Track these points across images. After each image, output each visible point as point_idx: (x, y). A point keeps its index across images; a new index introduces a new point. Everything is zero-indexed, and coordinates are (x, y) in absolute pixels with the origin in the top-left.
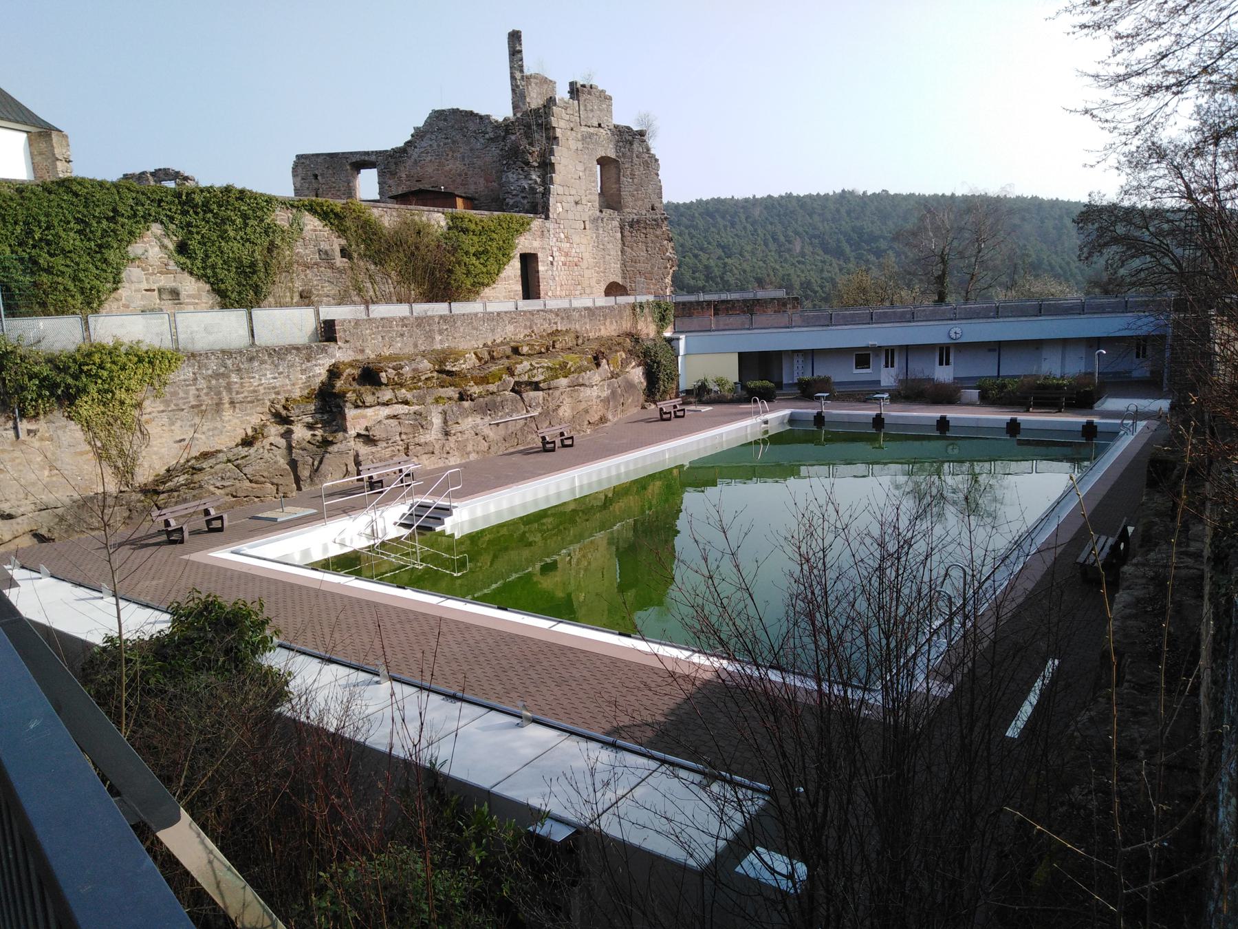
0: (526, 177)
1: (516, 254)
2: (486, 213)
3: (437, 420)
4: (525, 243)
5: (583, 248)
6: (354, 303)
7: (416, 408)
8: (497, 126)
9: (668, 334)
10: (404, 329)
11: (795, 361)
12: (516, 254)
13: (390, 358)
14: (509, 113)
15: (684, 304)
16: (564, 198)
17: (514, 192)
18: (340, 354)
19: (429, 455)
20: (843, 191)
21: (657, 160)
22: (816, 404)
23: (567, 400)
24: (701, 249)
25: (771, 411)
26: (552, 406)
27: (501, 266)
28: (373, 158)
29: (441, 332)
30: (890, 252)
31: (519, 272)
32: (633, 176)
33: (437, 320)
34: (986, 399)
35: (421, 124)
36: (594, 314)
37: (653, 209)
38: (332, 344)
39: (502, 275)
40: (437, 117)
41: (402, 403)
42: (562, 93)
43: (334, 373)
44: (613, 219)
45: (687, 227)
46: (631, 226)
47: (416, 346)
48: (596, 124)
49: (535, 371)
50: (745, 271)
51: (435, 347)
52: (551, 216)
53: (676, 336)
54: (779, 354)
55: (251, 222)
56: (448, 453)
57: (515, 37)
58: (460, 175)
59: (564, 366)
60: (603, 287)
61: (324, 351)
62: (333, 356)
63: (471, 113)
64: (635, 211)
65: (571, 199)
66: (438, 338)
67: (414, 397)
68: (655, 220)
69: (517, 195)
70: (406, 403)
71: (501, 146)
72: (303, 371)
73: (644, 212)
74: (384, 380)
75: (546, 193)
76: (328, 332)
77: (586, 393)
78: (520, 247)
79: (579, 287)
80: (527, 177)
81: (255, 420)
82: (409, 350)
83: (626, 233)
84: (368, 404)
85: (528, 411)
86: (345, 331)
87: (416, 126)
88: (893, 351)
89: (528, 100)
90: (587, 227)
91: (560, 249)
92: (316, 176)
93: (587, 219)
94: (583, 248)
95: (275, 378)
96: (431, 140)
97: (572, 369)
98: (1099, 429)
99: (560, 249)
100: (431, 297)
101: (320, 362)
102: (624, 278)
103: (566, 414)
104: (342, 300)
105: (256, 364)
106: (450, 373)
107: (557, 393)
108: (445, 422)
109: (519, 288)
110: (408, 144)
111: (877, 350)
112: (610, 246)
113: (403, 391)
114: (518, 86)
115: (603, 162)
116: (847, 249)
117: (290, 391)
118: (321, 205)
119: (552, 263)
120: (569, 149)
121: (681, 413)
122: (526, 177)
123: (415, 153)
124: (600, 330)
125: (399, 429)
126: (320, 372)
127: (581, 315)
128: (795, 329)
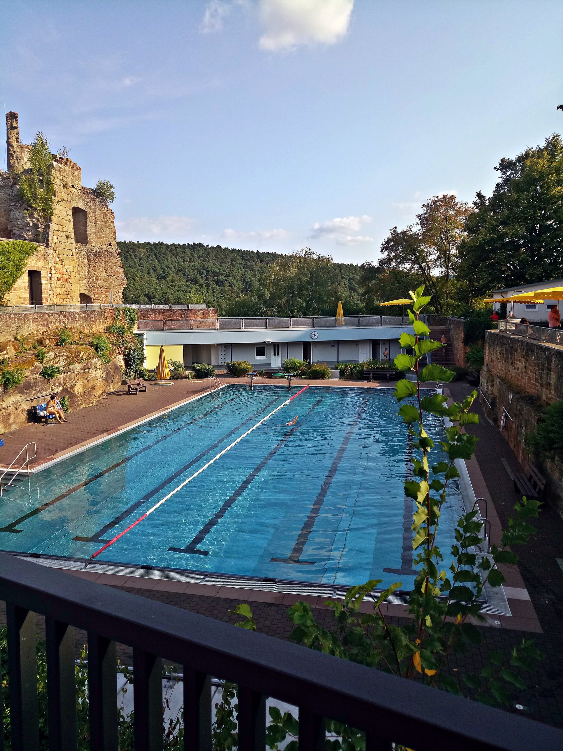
4: (32, 263)
9: (135, 330)
11: (220, 351)
12: (26, 270)
16: (59, 233)
17: (20, 226)
20: (194, 244)
23: (80, 381)
30: (226, 283)
31: (27, 284)
32: (96, 221)
34: (343, 375)
36: (88, 317)
39: (15, 286)
44: (82, 250)
46: (95, 255)
50: (137, 289)
52: (50, 245)
54: (208, 347)
65: (64, 234)
68: (111, 253)
78: (28, 265)
79: (69, 296)
83: (91, 260)
85: (52, 390)
91: (56, 269)
97: (84, 357)
99: (56, 269)
103: (79, 391)
107: (73, 375)
109: (27, 295)
111: (269, 344)
115: (76, 211)
116: (200, 279)
119: (50, 278)
124: (92, 327)
127: (80, 317)
128: (166, 331)
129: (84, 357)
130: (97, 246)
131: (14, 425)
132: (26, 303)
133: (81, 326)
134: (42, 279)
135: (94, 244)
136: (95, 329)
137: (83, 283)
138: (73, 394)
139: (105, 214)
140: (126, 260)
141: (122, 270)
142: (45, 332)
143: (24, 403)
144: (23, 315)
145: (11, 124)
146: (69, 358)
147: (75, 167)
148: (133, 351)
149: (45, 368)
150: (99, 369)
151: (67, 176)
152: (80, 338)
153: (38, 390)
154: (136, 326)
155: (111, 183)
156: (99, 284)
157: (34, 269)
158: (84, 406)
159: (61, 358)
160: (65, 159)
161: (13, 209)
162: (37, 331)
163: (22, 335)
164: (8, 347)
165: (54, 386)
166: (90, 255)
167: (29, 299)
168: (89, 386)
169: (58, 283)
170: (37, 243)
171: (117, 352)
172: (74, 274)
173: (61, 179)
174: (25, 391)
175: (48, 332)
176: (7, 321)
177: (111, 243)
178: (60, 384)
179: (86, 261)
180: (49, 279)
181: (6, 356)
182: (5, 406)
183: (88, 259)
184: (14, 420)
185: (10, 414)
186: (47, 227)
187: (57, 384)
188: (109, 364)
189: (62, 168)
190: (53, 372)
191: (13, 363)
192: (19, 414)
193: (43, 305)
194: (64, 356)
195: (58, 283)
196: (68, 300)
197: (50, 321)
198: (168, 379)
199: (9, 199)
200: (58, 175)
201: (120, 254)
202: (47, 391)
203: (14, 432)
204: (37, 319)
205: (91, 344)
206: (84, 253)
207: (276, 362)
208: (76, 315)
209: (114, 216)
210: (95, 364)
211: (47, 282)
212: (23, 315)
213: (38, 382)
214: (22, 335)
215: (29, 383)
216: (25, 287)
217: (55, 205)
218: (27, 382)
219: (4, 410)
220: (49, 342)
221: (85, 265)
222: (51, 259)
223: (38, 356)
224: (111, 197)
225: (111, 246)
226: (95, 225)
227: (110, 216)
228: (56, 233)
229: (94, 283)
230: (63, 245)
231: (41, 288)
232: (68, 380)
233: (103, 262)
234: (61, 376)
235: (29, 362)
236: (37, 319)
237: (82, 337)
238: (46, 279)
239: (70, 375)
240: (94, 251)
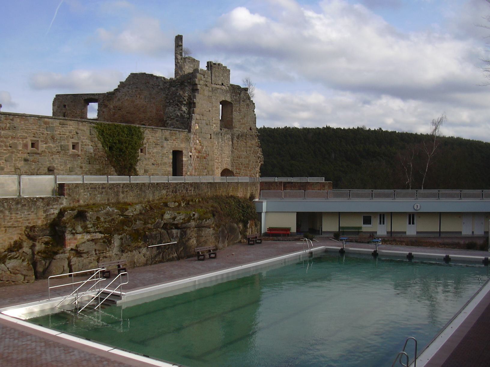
0: (179, 109)
6: (76, 174)
14: (173, 76)
15: (266, 183)
18: (65, 202)
21: (254, 104)
22: (373, 245)
25: (315, 246)
28: (97, 97)
29: (123, 192)
33: (122, 186)
35: (124, 80)
37: (250, 129)
40: (133, 77)
42: (203, 66)
43: (62, 213)
48: (221, 83)
57: (179, 39)
58: (142, 107)
62: (62, 204)
63: (152, 75)
69: (174, 119)
71: (166, 93)
75: (190, 118)
76: (61, 189)
79: (206, 171)
80: (180, 109)
81: (16, 238)
83: (235, 142)
88: (384, 215)
89: (184, 70)
90: (212, 137)
91: (195, 149)
92: (65, 106)
93: (212, 133)
95: (29, 214)
96: (129, 88)
98: (451, 259)
100: (120, 173)
101: (55, 207)
104: (71, 171)
105: (20, 206)
109: (171, 169)
110: (116, 90)
114: (178, 63)
120: (204, 95)
121: (213, 255)
122: (179, 109)
123: (119, 95)
126: (54, 211)
130: (240, 130)
134: (184, 157)
135: (238, 129)
139: (248, 105)
141: (260, 150)
145: (178, 44)
156: (240, 161)
167: (172, 172)
169: (197, 160)
177: (252, 127)
179: (231, 143)
183: (232, 141)
195: (197, 160)
207: (381, 230)
216: (169, 163)
225: (251, 130)
229: (237, 160)
238: (187, 157)
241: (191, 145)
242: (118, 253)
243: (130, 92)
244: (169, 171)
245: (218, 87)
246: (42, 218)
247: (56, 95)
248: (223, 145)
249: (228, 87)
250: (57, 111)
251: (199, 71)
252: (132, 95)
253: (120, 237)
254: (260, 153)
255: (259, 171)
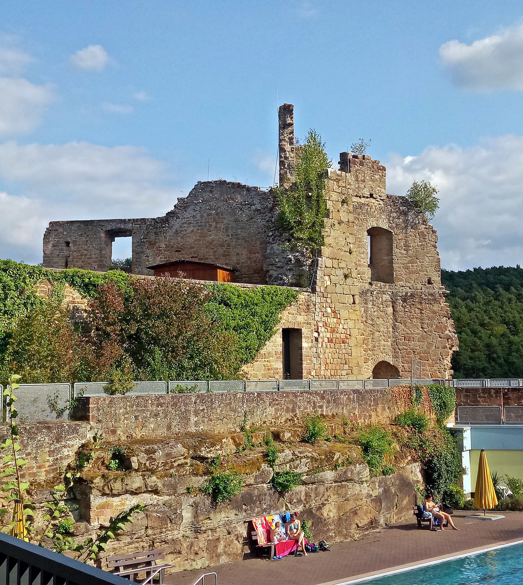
1: (279, 328)
2: (249, 285)
3: (187, 515)
5: (351, 324)
7: (166, 498)
8: (263, 196)
9: (450, 424)
10: (159, 408)
12: (279, 328)
13: (143, 441)
15: (467, 390)
17: (279, 264)
19: (175, 556)
24: (482, 325)
26: (313, 504)
27: (262, 340)
28: (129, 226)
29: (196, 413)
31: (280, 349)
32: (407, 247)
36: (363, 399)
38: (84, 424)
39: (262, 352)
41: (151, 492)
44: (384, 293)
45: (464, 299)
46: (404, 300)
47: (169, 428)
48: (367, 194)
49: (298, 462)
51: (189, 430)
52: (318, 289)
53: (459, 426)
55: (13, 293)
56: (197, 554)
58: (222, 245)
59: (329, 456)
60: (371, 366)
61: (75, 431)
62: (84, 437)
64: (408, 284)
65: (340, 273)
66: (193, 419)
67: (164, 485)
68: (432, 295)
70: (156, 492)
72: (51, 453)
73: (419, 286)
74: (135, 465)
77: (354, 489)
79: (346, 367)
82: (162, 432)
83: (399, 308)
84: (115, 492)
86: (99, 410)
87: (180, 197)
90: (357, 301)
91: (325, 325)
92: (68, 244)
94: (351, 324)
97: (340, 461)
99: (325, 325)
101: (70, 443)
102: (395, 357)
103: (331, 515)
106: (203, 459)
107: (322, 489)
108: (196, 516)
109: (279, 365)
112: (380, 321)
113: (154, 478)
115: (374, 232)
117: (35, 475)
118: (82, 276)
119: (317, 339)
123: (176, 224)
124: (370, 416)
125: (145, 522)
127: (349, 398)
129: (340, 461)
131: (223, 557)
132: (277, 377)
133: (350, 413)
134: (303, 340)
136: (374, 420)
137: (384, 345)
138: (321, 519)
139: (422, 235)
140: (518, 299)
141: (451, 321)
142: (290, 420)
143: (241, 525)
144: (256, 394)
146: (316, 461)
147: (375, 167)
148: (437, 457)
149: (278, 474)
150: (366, 481)
151: (349, 187)
152: (345, 433)
153: (265, 507)
154: (453, 415)
155: (433, 185)
156: (412, 347)
157: (291, 326)
158: (338, 540)
159: (302, 460)
160: (360, 156)
161: (271, 240)
162: (277, 418)
163: (253, 424)
164: (223, 440)
165: (290, 503)
166: (397, 299)
168: (348, 508)
169: (329, 346)
170: (297, 289)
171: (409, 458)
172: (355, 332)
173: (340, 191)
174: (244, 507)
175: (294, 421)
176: (231, 403)
177: (432, 279)
178: (299, 501)
179: (390, 310)
180: (314, 340)
181: (220, 452)
182: (211, 526)
183: (393, 307)
184: (224, 549)
185: (218, 539)
186: (314, 264)
187: (295, 500)
188: (391, 476)
189: (341, 176)
190: (288, 481)
191: (230, 464)
192: (232, 541)
193: (304, 380)
194: (307, 457)
195: (329, 346)
196: (344, 373)
197: (298, 403)
198: (492, 510)
199: (268, 226)
200: (335, 187)
201: (446, 296)
202: (278, 509)
203: (222, 567)
204: (277, 400)
205: (356, 442)
206: (386, 297)
208: (342, 396)
209: (436, 236)
210: (359, 473)
211: (310, 345)
212: (256, 394)
213: (265, 495)
214: (253, 424)
215: (251, 495)
217: (326, 231)
218: (248, 493)
219: (210, 533)
220: (290, 435)
221: (389, 316)
222: (318, 310)
223: (267, 455)
224: (432, 206)
225: (432, 284)
226: (405, 252)
227: (430, 237)
228: (327, 271)
230: (339, 289)
231: (301, 355)
232: (313, 495)
233: (417, 311)
234: (303, 488)
235: (253, 463)
236: (277, 400)
237: (348, 430)
238: (310, 340)
239: (316, 489)
240: (404, 294)
241: (317, 318)
242: (188, 533)
243: (198, 217)
244: (277, 369)
245: (363, 202)
246: (47, 466)
247: (51, 223)
248: (375, 313)
249: (382, 200)
250: (51, 253)
251: (329, 174)
252: (201, 222)
253: (191, 501)
254: (450, 329)
255: (450, 365)
